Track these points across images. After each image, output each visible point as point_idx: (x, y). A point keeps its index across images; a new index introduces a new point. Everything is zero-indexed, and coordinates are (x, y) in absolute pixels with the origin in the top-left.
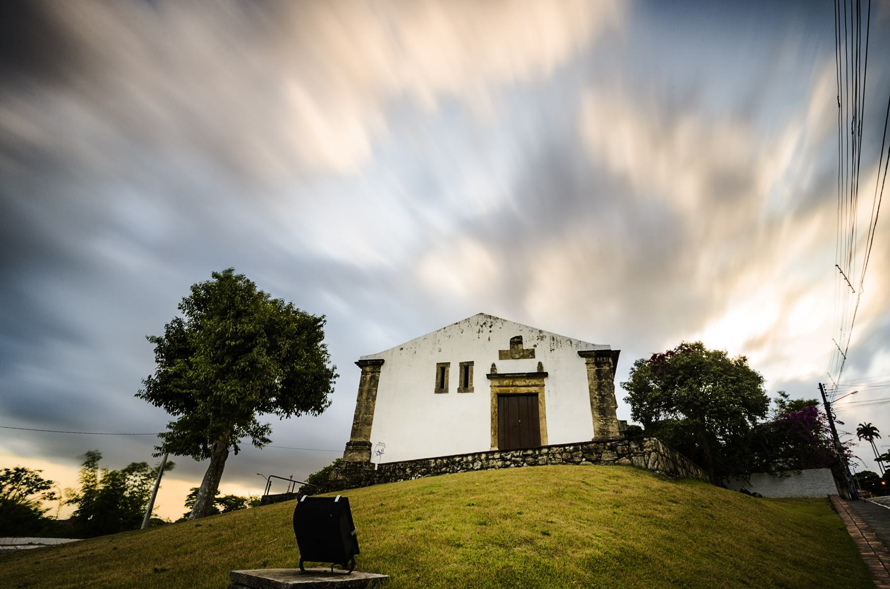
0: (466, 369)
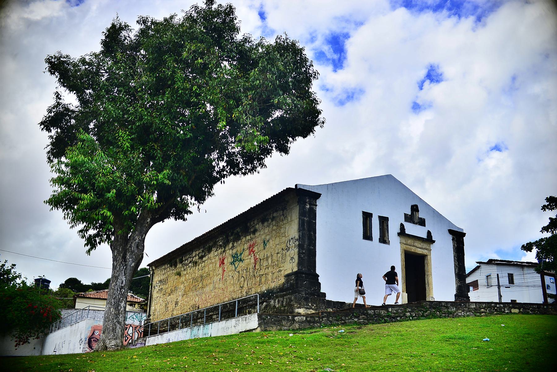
0: (384, 221)
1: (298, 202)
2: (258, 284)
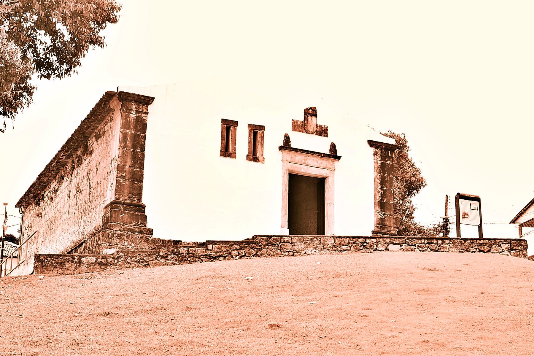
0: (256, 131)
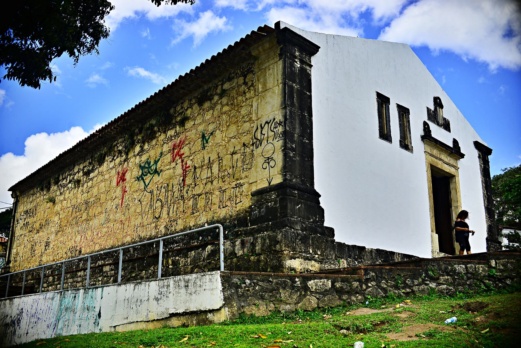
0: (404, 112)
1: (280, 55)
2: (190, 211)
